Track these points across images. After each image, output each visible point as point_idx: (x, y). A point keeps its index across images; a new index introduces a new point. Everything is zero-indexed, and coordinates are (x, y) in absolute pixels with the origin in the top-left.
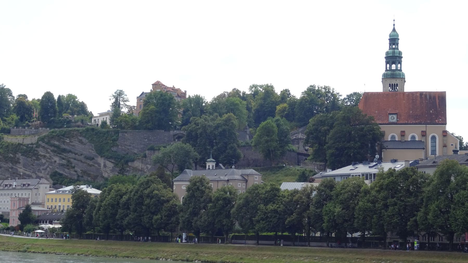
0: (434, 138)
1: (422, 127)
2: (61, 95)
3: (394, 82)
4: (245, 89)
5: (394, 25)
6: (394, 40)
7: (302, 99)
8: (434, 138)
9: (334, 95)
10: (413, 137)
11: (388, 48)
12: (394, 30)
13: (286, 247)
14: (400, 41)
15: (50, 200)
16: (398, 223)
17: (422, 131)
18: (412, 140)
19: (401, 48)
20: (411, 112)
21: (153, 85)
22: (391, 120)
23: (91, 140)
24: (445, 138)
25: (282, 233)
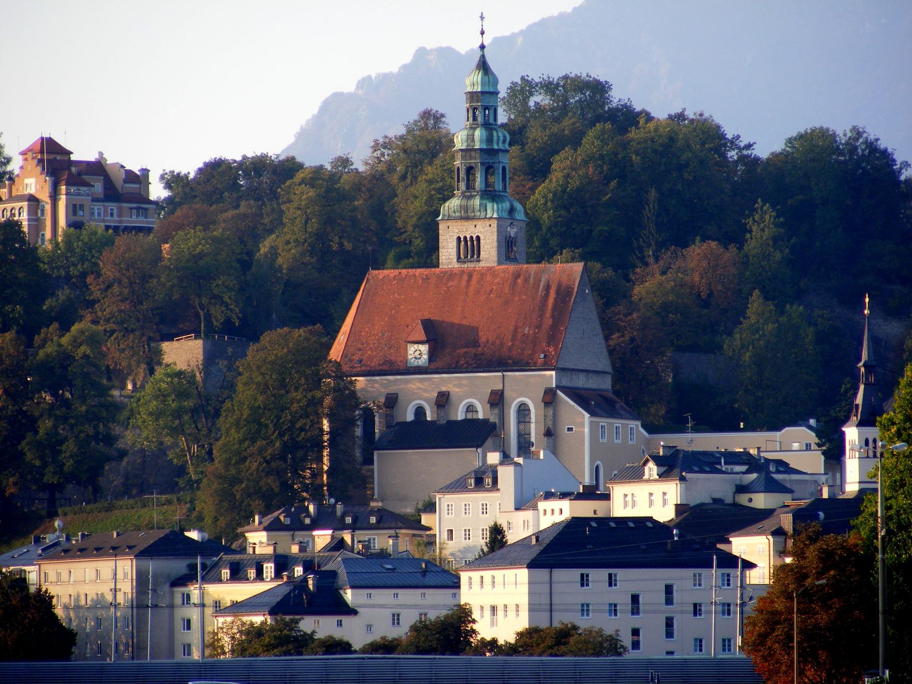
0: (523, 410)
1: (491, 380)
2: (46, 135)
4: (349, 87)
6: (482, 587)
7: (768, 159)
8: (523, 410)
9: (871, 143)
10: (470, 408)
13: (455, 243)
15: (549, 512)
16: (603, 107)
21: (518, 634)
23: (235, 186)
25: (326, 472)
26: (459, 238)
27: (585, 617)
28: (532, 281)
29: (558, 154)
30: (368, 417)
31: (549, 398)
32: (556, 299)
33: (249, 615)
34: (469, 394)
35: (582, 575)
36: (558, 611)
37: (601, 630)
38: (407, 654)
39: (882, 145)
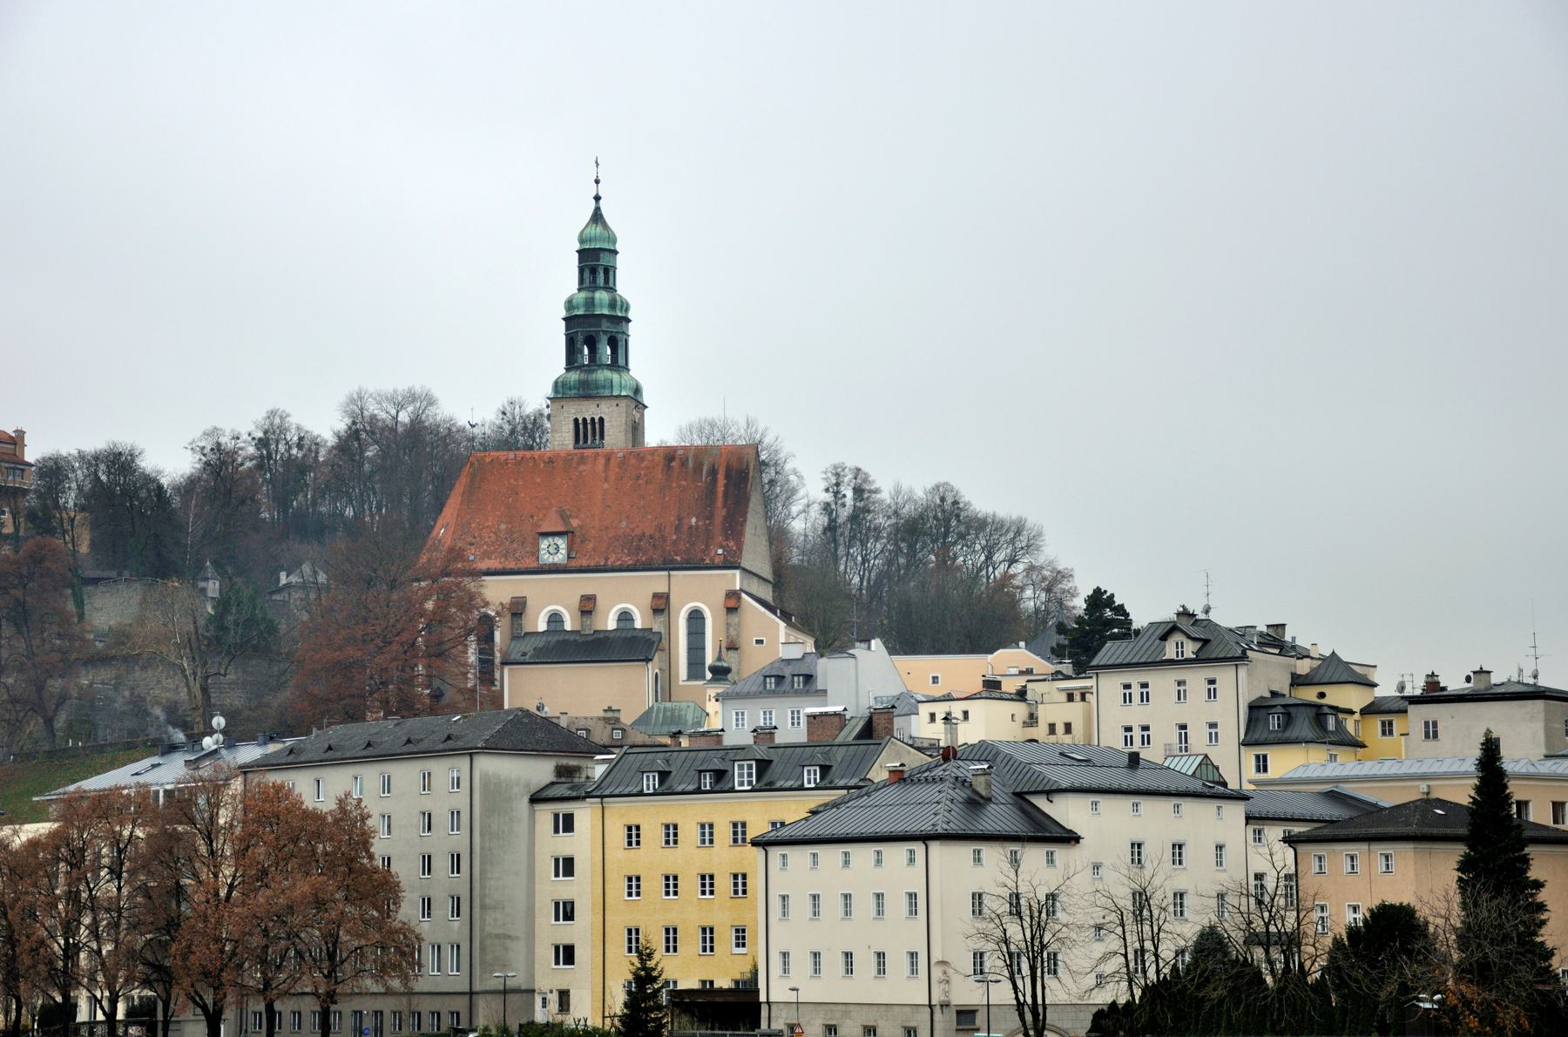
0: (696, 618)
1: (655, 581)
3: (589, 411)
5: (597, 198)
6: (595, 263)
8: (696, 618)
11: (576, 285)
12: (597, 217)
14: (621, 262)
17: (656, 596)
18: (622, 625)
19: (625, 285)
20: (624, 524)
21: (1498, 740)
22: (546, 558)
24: (734, 619)
26: (576, 420)
27: (707, 896)
28: (691, 464)
29: (708, 989)
30: (487, 624)
31: (732, 605)
32: (726, 486)
33: (333, 757)
34: (622, 599)
35: (1265, 770)
36: (532, 977)
37: (968, 503)
38: (481, 834)
39: (549, 392)
